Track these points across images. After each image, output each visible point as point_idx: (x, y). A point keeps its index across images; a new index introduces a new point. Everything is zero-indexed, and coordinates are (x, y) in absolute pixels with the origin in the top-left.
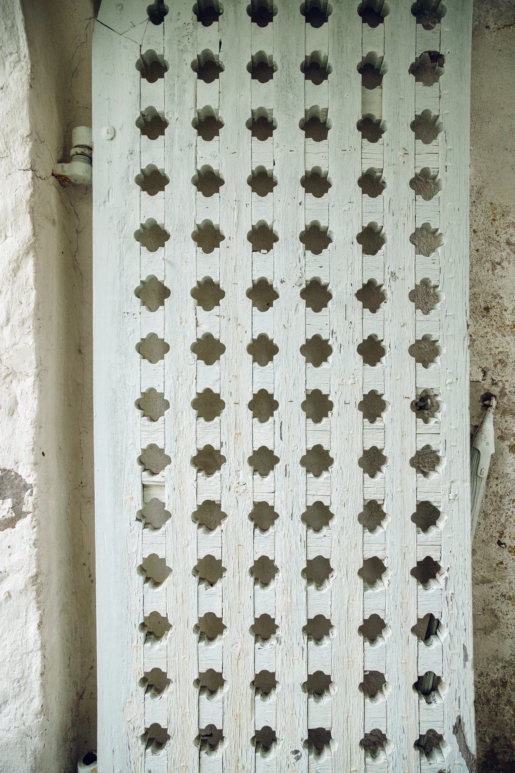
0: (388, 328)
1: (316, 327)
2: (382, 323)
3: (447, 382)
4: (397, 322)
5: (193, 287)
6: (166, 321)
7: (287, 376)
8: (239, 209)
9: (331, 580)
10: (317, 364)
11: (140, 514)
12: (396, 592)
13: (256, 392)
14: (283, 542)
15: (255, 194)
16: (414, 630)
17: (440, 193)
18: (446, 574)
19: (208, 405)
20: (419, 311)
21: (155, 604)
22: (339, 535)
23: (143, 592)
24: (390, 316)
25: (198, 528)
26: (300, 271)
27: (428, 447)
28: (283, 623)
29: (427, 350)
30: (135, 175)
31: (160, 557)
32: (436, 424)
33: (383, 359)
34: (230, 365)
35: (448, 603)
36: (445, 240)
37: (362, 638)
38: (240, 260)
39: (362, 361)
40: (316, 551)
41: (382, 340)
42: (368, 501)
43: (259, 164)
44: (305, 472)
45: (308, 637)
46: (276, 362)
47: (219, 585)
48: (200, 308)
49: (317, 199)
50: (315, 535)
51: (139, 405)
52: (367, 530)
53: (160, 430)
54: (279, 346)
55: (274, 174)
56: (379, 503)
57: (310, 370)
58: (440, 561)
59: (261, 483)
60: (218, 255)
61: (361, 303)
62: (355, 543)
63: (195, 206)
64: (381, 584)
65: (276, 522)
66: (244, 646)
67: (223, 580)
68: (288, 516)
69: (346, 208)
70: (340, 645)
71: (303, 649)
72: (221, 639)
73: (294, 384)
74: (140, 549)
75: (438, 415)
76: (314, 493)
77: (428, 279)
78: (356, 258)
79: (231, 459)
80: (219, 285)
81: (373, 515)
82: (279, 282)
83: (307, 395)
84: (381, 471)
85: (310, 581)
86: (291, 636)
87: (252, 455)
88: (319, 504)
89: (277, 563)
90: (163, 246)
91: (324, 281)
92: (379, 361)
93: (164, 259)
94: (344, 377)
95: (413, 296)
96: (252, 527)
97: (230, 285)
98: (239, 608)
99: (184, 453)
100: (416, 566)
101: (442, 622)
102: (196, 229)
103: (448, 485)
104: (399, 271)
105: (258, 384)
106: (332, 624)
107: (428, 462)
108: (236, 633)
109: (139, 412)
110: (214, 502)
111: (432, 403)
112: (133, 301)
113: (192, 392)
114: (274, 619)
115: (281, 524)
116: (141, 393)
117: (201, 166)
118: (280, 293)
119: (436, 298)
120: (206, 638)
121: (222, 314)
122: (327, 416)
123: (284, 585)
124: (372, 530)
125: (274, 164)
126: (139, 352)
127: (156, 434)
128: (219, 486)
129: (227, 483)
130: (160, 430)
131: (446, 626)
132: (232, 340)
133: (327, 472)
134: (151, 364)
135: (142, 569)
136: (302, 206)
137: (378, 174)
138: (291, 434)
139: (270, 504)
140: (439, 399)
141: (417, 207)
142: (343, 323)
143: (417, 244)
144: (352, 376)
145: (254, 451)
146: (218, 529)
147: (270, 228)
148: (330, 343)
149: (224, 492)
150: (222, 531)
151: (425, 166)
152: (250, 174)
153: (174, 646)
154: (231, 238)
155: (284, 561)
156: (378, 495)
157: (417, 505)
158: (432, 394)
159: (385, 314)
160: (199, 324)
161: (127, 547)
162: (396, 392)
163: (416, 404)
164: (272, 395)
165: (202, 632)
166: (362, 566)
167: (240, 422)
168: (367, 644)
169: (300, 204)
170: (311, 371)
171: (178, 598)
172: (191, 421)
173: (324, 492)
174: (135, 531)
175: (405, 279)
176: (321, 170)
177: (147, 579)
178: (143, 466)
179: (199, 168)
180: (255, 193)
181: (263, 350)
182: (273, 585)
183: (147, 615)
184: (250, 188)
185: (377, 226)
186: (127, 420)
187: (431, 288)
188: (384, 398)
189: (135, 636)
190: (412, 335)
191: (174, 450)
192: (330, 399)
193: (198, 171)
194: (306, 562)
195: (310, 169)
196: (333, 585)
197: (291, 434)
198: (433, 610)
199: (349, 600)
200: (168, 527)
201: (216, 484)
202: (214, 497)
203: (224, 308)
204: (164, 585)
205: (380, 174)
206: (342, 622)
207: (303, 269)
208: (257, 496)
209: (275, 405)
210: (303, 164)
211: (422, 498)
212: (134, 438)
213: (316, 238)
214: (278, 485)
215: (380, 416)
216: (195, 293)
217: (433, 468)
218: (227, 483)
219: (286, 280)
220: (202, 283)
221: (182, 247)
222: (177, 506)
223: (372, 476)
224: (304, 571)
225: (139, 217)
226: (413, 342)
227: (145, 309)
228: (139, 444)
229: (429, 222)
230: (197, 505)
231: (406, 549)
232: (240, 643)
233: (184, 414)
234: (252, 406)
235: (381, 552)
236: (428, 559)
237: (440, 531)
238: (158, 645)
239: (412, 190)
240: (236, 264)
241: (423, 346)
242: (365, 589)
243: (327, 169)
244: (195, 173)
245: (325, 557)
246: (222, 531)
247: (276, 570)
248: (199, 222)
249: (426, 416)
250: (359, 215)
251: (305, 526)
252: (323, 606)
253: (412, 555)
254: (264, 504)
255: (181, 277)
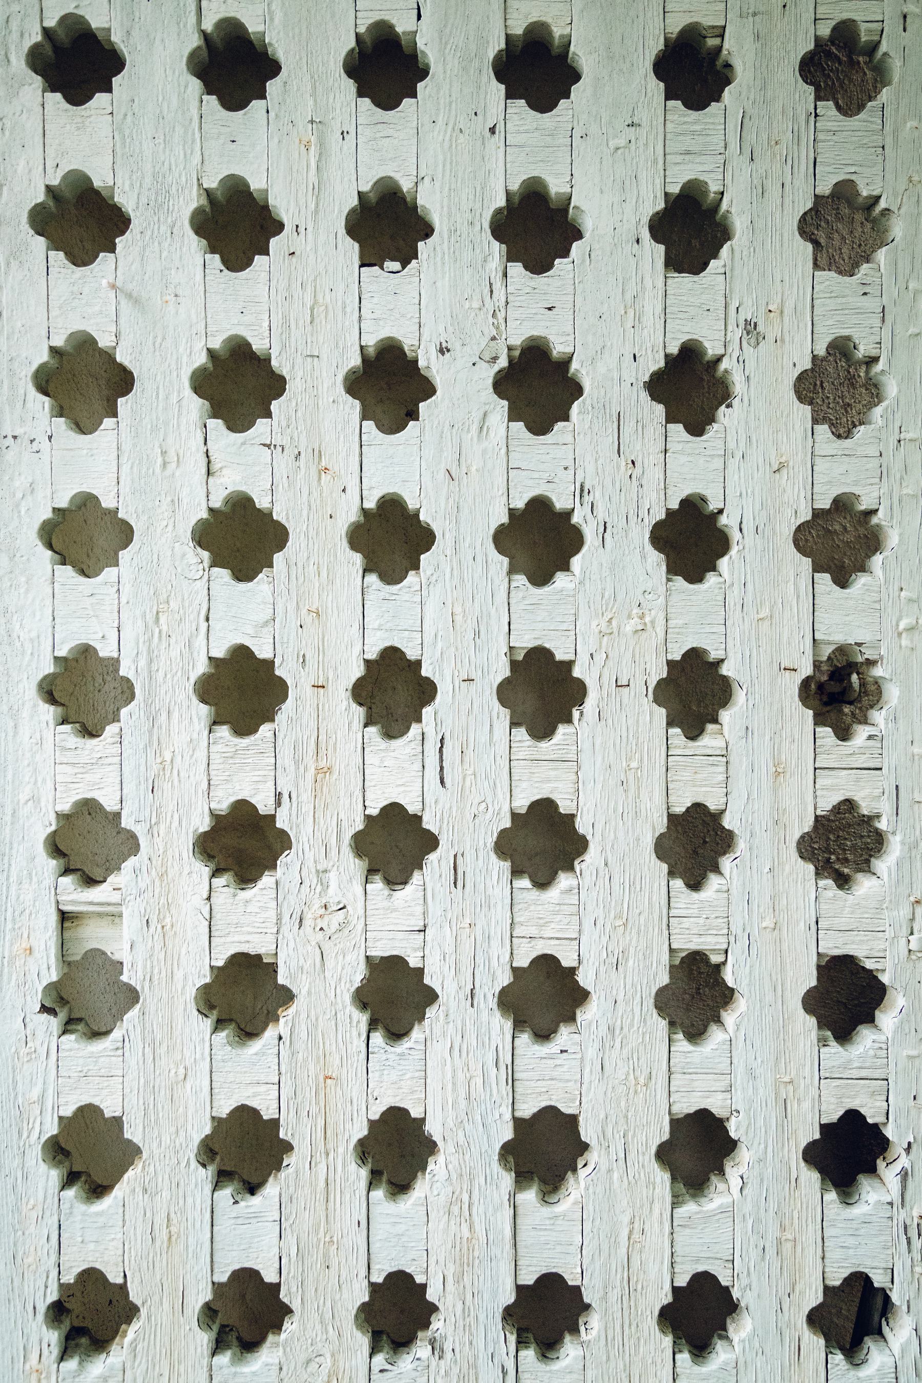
0: (736, 477)
1: (536, 475)
2: (719, 463)
3: (902, 626)
4: (761, 461)
5: (197, 365)
6: (123, 459)
7: (458, 610)
8: (322, 144)
9: (582, 1173)
10: (541, 578)
11: (54, 994)
12: (762, 1211)
13: (372, 655)
14: (448, 1068)
15: (366, 102)
16: (815, 1319)
17: (885, 95)
18: (904, 1161)
19: (243, 691)
20: (823, 430)
21: (92, 1246)
22: (602, 1048)
23: (60, 1215)
24: (742, 444)
25: (215, 1030)
26: (491, 320)
27: (848, 805)
28: (450, 1298)
29: (847, 537)
30: (28, 43)
31: (108, 1114)
32: (871, 743)
33: (724, 563)
34: (301, 580)
35: (909, 1243)
36: (898, 229)
37: (668, 1341)
38: (328, 291)
39: (664, 568)
40: (540, 1094)
41: (721, 511)
42: (684, 954)
43: (375, 17)
44: (507, 874)
45: (519, 1336)
46: (429, 573)
47: (271, 1189)
48: (217, 425)
49: (539, 115)
50: (536, 1047)
51: (50, 692)
52: (680, 1036)
53: (109, 760)
54: (435, 527)
55: (420, 45)
56: (715, 959)
57: (521, 594)
58: (885, 1124)
59: (386, 904)
60: (264, 276)
61: (660, 409)
62: (646, 1073)
63: (197, 135)
64: (721, 1186)
65: (430, 1012)
66: (341, 1364)
67: (283, 1174)
68: (462, 996)
69: (622, 142)
70: (608, 1359)
71: (504, 1372)
72: (277, 1345)
73: (477, 634)
74: (50, 1092)
75: (878, 716)
76: (533, 931)
77: (848, 338)
78: (648, 283)
79: (306, 839)
80: (268, 360)
81: (696, 993)
82: (433, 352)
83: (514, 664)
84: (720, 873)
85: (523, 1178)
86: (471, 1334)
87: (361, 827)
88: (546, 964)
89: (433, 1128)
90: (112, 249)
91: (558, 349)
92: (714, 569)
93: (113, 286)
94: (615, 613)
95: (808, 387)
96: (364, 1027)
97: (299, 360)
98: (326, 1256)
99: (175, 824)
100: (817, 1136)
101: (895, 1297)
102: (204, 201)
103: (904, 912)
104: (766, 319)
105: (379, 633)
106: (587, 1300)
107: (854, 846)
108: (318, 1327)
109: (49, 712)
110: (259, 957)
111: (863, 684)
112: (29, 405)
113: (195, 654)
114: (424, 1287)
115: (442, 1017)
116: (56, 658)
117: (214, 21)
118: (438, 381)
119: (874, 392)
120: (235, 1342)
121: (278, 440)
122: (569, 720)
123: (450, 1189)
124: (695, 1035)
125: (419, 17)
126: (50, 546)
127: (96, 770)
128: (272, 914)
129: (292, 904)
130: (109, 760)
131: (905, 1308)
132: (305, 513)
133: (570, 875)
134: (83, 579)
135: (57, 1150)
136: (498, 138)
137: (712, 42)
138: (469, 769)
139: (414, 962)
140: (878, 671)
141: (821, 136)
142: (612, 462)
143: (822, 241)
144: (636, 611)
145: (368, 818)
146: (270, 1033)
147: (408, 199)
148: (576, 519)
149: (285, 929)
150: (280, 1038)
151: (845, 16)
152: (352, 43)
153: (143, 1367)
154: (301, 229)
155: (450, 1123)
156: (709, 939)
157: (819, 967)
158: (860, 659)
159: (729, 438)
160: (215, 467)
161: (15, 1089)
162: (759, 653)
163: (821, 687)
164: (418, 663)
165: (223, 1327)
166: (666, 1136)
167: (328, 737)
168: (684, 1357)
169: (492, 130)
170: (524, 598)
171: (156, 1227)
172: (195, 736)
173: (561, 930)
174: (38, 1043)
175: (783, 340)
176: (550, 34)
177: (71, 1179)
178: (62, 861)
179: (208, 25)
180: (367, 101)
181: (392, 539)
182: (421, 1188)
183: (69, 1278)
184: (350, 86)
185: (706, 192)
186: (16, 734)
187: (860, 363)
188: (725, 670)
189: (34, 1339)
190: (802, 495)
191: (147, 814)
192: (577, 673)
193: (205, 35)
194: (511, 1124)
195: (518, 29)
196: (587, 1189)
197: (469, 769)
198: (869, 1263)
199: (631, 1232)
200: (131, 1028)
201: (265, 908)
202: (259, 946)
203: (284, 424)
204: (118, 1192)
205: (717, 41)
206: (614, 1296)
207: (501, 316)
208: (376, 940)
209: (426, 691)
210: (499, 15)
211: (834, 946)
212: (36, 783)
213: (536, 228)
214: (435, 909)
215: (715, 721)
216: (202, 383)
217: (865, 866)
218: (292, 904)
219: (455, 345)
220: (224, 355)
221: (165, 254)
222: (156, 971)
223: (695, 885)
224: (507, 1150)
225: (41, 167)
226: (806, 515)
227: (64, 427)
228: (51, 799)
229: (853, 177)
230: (212, 967)
231: (790, 1088)
232: (328, 1356)
233: (175, 715)
234: (362, 692)
235: (720, 1096)
236: (853, 1117)
237: (884, 1038)
238: (99, 1366)
239: (806, 86)
240: (316, 302)
241: (837, 527)
242: (676, 1202)
243: (567, 31)
244: (195, 41)
245: (567, 1109)
246: (280, 1038)
247: (431, 1147)
248: (212, 183)
249: (848, 720)
250: (655, 161)
251: (508, 1025)
252: (559, 1249)
253: (806, 1105)
254: (395, 964)
255: (164, 339)
